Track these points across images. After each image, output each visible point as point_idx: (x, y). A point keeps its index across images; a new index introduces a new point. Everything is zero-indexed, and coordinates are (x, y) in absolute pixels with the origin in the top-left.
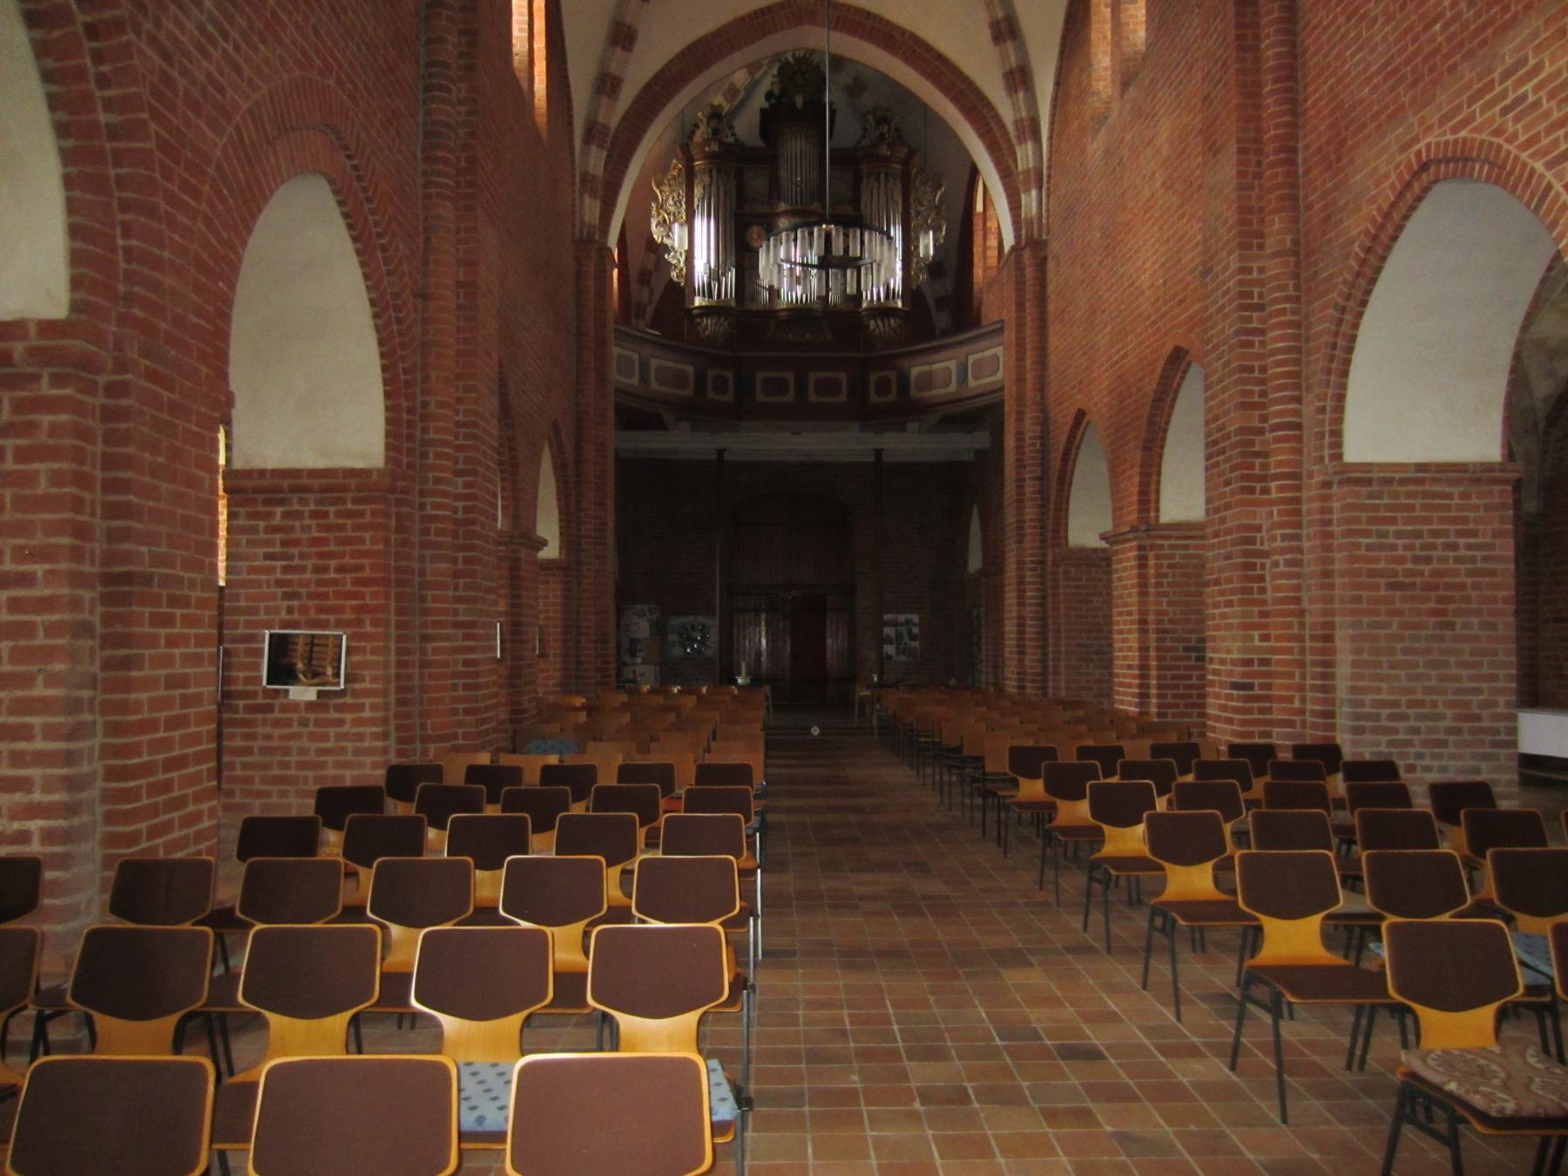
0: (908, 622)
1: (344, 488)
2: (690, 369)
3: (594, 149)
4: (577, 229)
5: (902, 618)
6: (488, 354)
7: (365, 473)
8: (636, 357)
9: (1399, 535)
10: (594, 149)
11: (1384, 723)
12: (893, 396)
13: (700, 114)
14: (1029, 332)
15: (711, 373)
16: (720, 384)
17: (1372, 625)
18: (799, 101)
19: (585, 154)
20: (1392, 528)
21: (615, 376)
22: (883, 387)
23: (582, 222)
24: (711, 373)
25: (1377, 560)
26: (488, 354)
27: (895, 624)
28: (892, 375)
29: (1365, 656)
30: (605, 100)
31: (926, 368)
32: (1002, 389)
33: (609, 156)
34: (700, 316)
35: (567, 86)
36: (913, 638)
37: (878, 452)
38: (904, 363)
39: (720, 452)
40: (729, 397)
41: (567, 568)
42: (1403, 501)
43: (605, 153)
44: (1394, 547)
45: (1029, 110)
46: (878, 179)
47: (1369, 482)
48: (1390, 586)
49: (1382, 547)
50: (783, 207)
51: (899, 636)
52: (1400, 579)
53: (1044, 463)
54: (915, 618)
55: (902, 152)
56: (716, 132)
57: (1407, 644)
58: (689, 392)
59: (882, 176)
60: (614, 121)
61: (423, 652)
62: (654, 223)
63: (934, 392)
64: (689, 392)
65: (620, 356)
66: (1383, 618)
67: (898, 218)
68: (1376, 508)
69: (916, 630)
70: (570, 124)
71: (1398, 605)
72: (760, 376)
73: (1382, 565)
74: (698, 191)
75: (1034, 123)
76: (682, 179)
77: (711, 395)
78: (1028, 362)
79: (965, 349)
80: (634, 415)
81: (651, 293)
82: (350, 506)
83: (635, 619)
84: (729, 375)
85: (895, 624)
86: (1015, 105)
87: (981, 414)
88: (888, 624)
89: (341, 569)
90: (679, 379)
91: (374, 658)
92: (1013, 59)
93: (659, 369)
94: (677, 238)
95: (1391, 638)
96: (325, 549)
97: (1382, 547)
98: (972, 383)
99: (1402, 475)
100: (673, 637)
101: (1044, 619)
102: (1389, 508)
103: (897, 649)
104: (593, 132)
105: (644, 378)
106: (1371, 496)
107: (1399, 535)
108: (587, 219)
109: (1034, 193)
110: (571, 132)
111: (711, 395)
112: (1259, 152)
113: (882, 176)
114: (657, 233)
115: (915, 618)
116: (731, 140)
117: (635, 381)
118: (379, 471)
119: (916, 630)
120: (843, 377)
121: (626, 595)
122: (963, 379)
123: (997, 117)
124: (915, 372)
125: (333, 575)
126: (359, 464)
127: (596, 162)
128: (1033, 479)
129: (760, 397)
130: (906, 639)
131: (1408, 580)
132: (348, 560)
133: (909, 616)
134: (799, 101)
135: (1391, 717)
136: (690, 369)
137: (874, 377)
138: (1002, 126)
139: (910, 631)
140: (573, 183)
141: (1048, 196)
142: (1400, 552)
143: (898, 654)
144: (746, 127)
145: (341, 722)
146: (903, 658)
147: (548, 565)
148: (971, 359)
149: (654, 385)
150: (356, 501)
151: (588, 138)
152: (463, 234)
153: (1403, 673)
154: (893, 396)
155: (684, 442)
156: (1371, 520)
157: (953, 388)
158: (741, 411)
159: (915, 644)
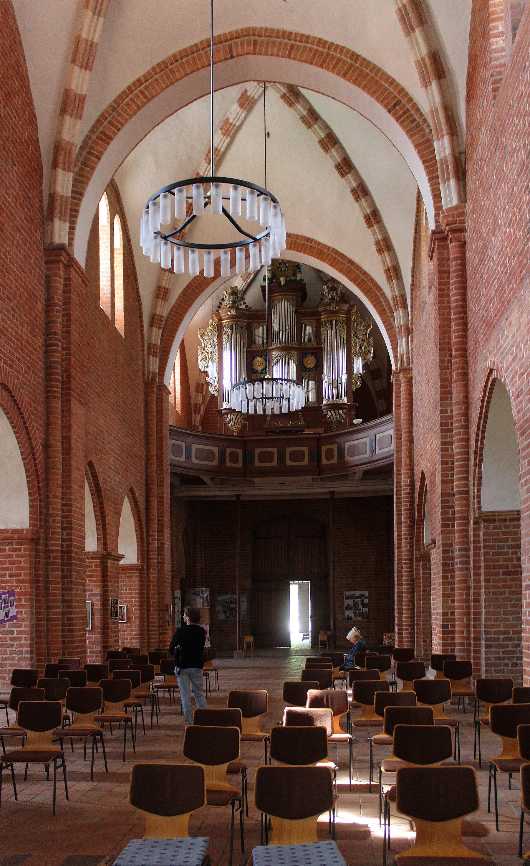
0: (361, 596)
1: (12, 538)
2: (216, 450)
3: (155, 329)
4: (146, 377)
5: (357, 594)
6: (79, 469)
7: (22, 531)
8: (183, 444)
9: (509, 547)
10: (155, 329)
11: (501, 642)
12: (335, 460)
13: (225, 293)
14: (403, 422)
15: (229, 450)
16: (234, 458)
17: (495, 593)
18: (282, 280)
19: (150, 332)
20: (506, 544)
21: (169, 457)
22: (330, 454)
23: (149, 372)
24: (229, 450)
25: (499, 560)
26: (79, 469)
27: (353, 597)
28: (334, 447)
29: (492, 609)
30: (160, 302)
31: (353, 443)
32: (392, 455)
33: (163, 332)
34: (226, 414)
35: (139, 296)
36: (364, 606)
37: (332, 493)
38: (340, 440)
39: (238, 496)
40: (240, 465)
41: (143, 569)
42: (511, 529)
43: (161, 331)
44: (507, 553)
45: (399, 291)
46: (331, 324)
47: (494, 521)
48: (504, 573)
49: (501, 554)
50: (275, 345)
51: (356, 605)
52: (510, 569)
53: (412, 502)
54: (366, 593)
55: (345, 307)
56: (234, 302)
57: (513, 602)
58: (216, 463)
59: (334, 322)
60: (165, 314)
61: (48, 614)
62: (200, 358)
63: (358, 457)
64: (216, 463)
65: (173, 445)
66: (502, 590)
67: (345, 371)
68: (498, 534)
69: (366, 601)
70: (141, 317)
71: (509, 583)
72: (257, 451)
73: (501, 563)
74: (225, 338)
75: (403, 297)
76: (216, 332)
77: (229, 464)
78: (403, 439)
79: (375, 431)
80: (185, 478)
81: (337, 293)
82: (15, 546)
83: (193, 597)
84: (240, 451)
85: (353, 597)
86: (392, 288)
87: (384, 471)
88: (348, 597)
89: (11, 575)
90: (210, 456)
91: (25, 616)
92: (389, 262)
93: (197, 450)
94: (212, 370)
95: (504, 599)
96: (5, 566)
97: (501, 554)
98: (378, 451)
99: (511, 517)
100: (219, 608)
101: (413, 593)
102: (504, 533)
103: (355, 614)
104: (154, 320)
105: (188, 456)
106: (495, 528)
107: (509, 547)
108: (151, 370)
109: (404, 339)
110: (142, 322)
111: (229, 464)
112: (450, 350)
113: (334, 322)
114: (201, 365)
115: (366, 593)
116: (243, 307)
117: (183, 459)
118: (27, 530)
119: (366, 601)
120: (306, 449)
121: (186, 584)
122: (373, 450)
123: (383, 294)
124: (347, 445)
125: (8, 578)
126: (18, 527)
127: (156, 337)
128: (405, 510)
129: (258, 464)
130: (360, 606)
131: (514, 570)
132: (14, 571)
133: (362, 592)
134: (282, 280)
135: (504, 639)
136: (216, 450)
137: (324, 448)
138: (386, 300)
139: (362, 602)
140: (143, 350)
141: (412, 341)
142: (510, 556)
143: (355, 616)
144: (253, 297)
145: (12, 646)
146: (359, 619)
147: (130, 568)
148: (378, 436)
149: (194, 460)
150: (18, 544)
151: (151, 325)
152: (65, 413)
153: (511, 617)
154: (335, 460)
155: (212, 491)
156: (495, 540)
157: (368, 454)
158: (247, 472)
159: (366, 610)
